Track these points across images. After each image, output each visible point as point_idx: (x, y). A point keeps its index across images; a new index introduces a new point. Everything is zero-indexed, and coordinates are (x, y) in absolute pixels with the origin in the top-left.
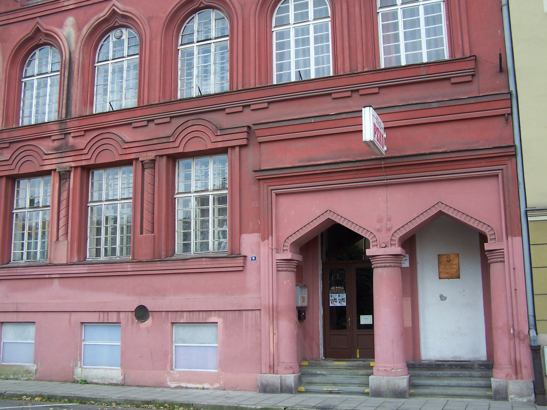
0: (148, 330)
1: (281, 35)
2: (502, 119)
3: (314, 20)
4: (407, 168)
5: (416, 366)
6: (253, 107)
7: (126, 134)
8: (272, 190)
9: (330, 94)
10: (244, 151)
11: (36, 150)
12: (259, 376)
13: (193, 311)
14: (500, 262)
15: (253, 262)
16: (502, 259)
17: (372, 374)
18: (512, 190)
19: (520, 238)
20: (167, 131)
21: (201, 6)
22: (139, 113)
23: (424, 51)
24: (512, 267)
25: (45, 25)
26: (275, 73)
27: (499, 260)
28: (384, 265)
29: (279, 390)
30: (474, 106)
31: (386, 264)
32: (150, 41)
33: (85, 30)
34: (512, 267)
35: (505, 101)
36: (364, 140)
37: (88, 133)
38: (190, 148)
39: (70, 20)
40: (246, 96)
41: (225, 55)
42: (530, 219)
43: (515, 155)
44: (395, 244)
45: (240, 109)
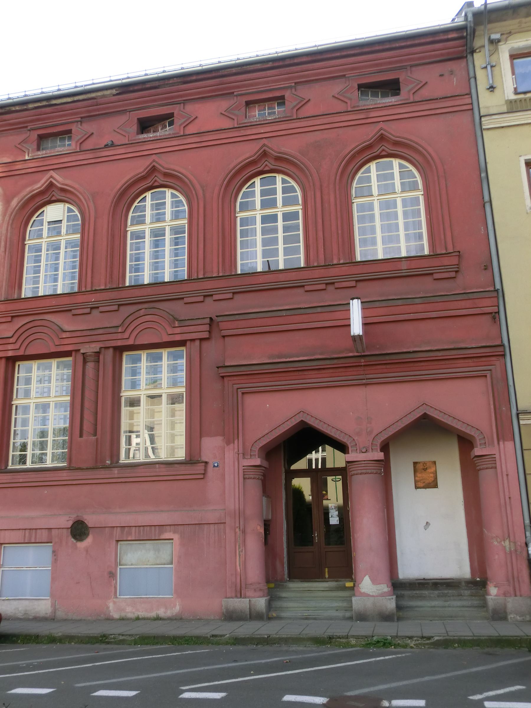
0: (87, 550)
1: (244, 222)
2: (488, 317)
4: (388, 366)
5: (399, 586)
6: (216, 297)
7: (63, 322)
8: (238, 389)
9: (303, 286)
10: (205, 344)
12: (224, 601)
15: (215, 468)
16: (493, 465)
17: (354, 595)
18: (502, 392)
19: (512, 443)
20: (115, 320)
21: (154, 185)
22: (80, 299)
23: (403, 244)
24: (505, 474)
26: (239, 262)
27: (490, 466)
28: (364, 471)
29: (249, 616)
30: (460, 302)
31: (368, 471)
32: (96, 218)
33: (14, 202)
34: (505, 474)
35: (492, 299)
36: (352, 334)
37: (15, 320)
40: (208, 285)
41: (179, 240)
42: (522, 422)
43: (504, 356)
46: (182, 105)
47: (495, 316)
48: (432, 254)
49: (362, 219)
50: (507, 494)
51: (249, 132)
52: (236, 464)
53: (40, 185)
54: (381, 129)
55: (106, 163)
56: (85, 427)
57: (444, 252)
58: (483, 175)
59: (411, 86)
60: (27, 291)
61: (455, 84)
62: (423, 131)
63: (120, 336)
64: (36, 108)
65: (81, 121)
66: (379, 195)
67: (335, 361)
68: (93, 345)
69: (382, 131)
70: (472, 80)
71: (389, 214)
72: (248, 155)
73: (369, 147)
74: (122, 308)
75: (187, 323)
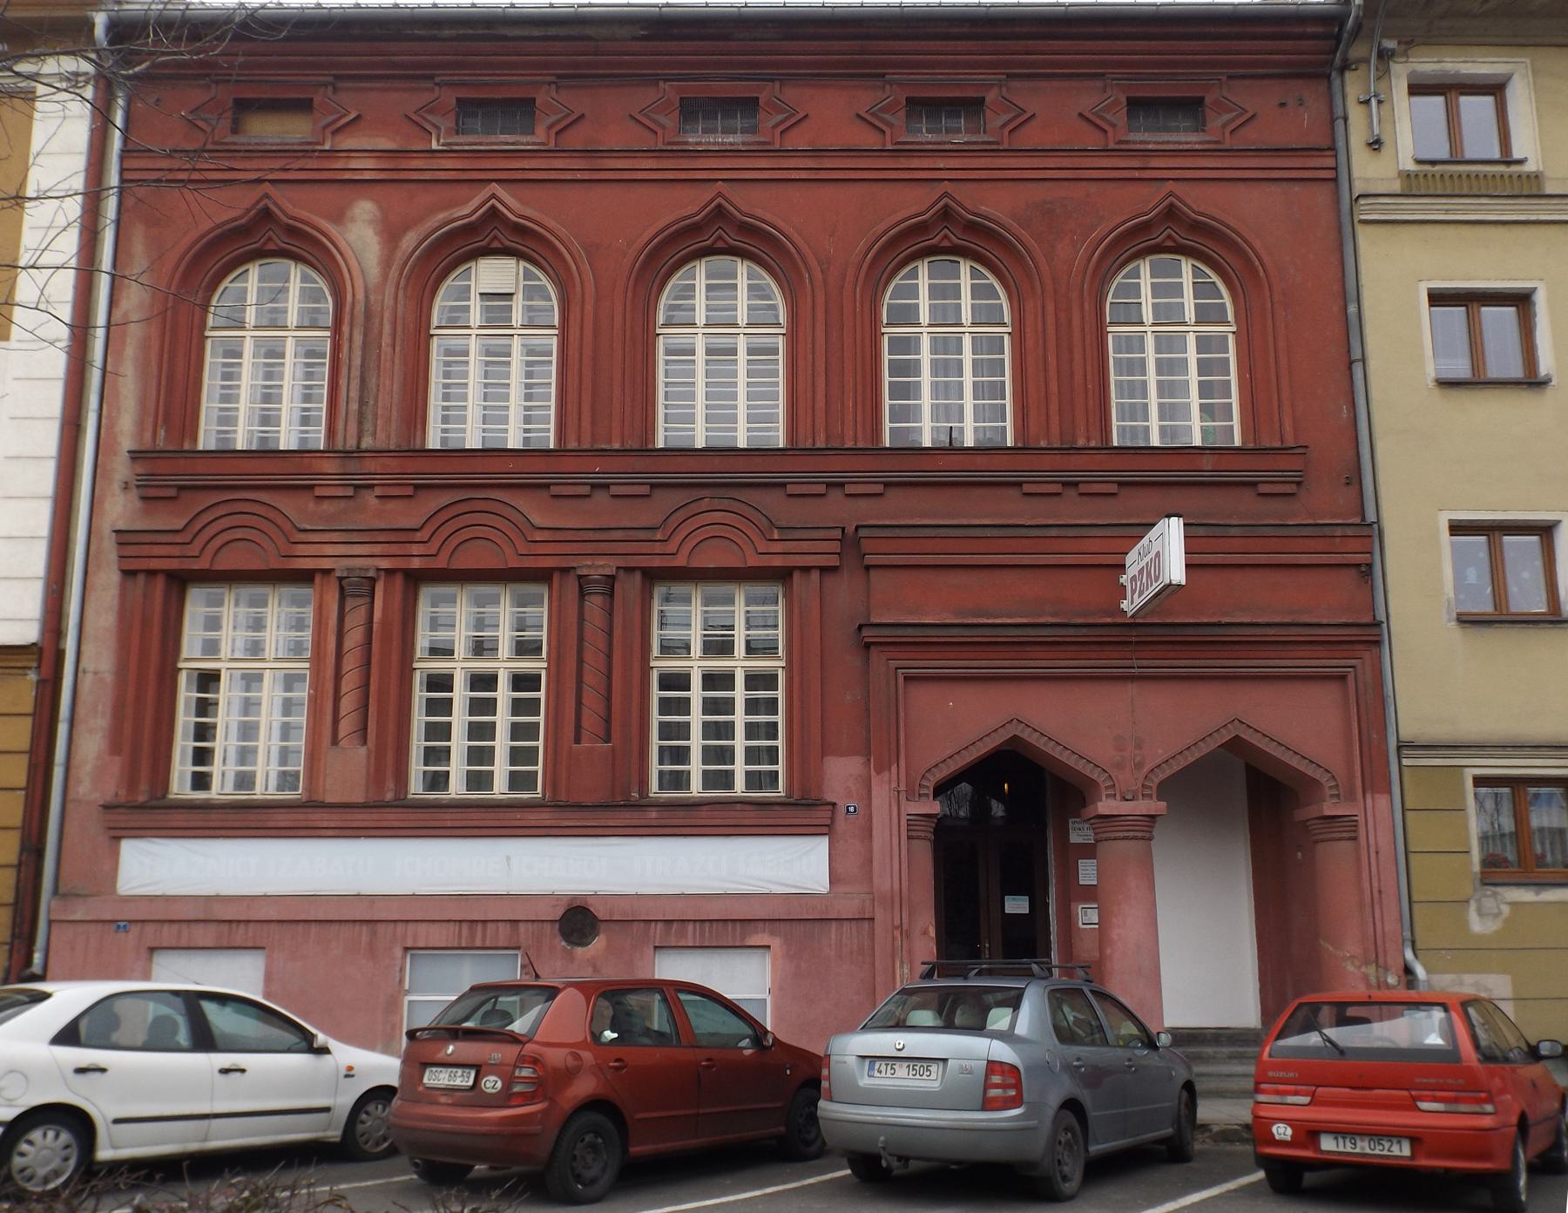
2: (1353, 571)
3: (974, 324)
7: (537, 512)
10: (830, 581)
11: (271, 514)
13: (230, 921)
14: (1142, 838)
15: (850, 816)
18: (1371, 707)
20: (409, 515)
25: (293, 204)
26: (887, 425)
30: (1307, 541)
33: (409, 241)
38: (225, 563)
39: (364, 210)
40: (837, 463)
42: (1405, 762)
43: (1378, 643)
44: (1150, 796)
45: (822, 489)
46: (777, 84)
47: (1365, 572)
48: (1251, 445)
49: (897, 369)
50: (1375, 884)
51: (915, 163)
52: (895, 809)
53: (468, 208)
54: (1171, 194)
55: (1010, 184)
56: (585, 723)
57: (1277, 444)
58: (1352, 309)
59: (553, 118)
60: (207, 439)
61: (1302, 124)
62: (1249, 209)
63: (658, 548)
64: (458, 38)
65: (332, 84)
66: (707, 325)
67: (1084, 631)
68: (601, 561)
69: (720, 200)
70: (1340, 123)
71: (947, 368)
72: (913, 210)
73: (1144, 228)
74: (658, 493)
75: (798, 535)
